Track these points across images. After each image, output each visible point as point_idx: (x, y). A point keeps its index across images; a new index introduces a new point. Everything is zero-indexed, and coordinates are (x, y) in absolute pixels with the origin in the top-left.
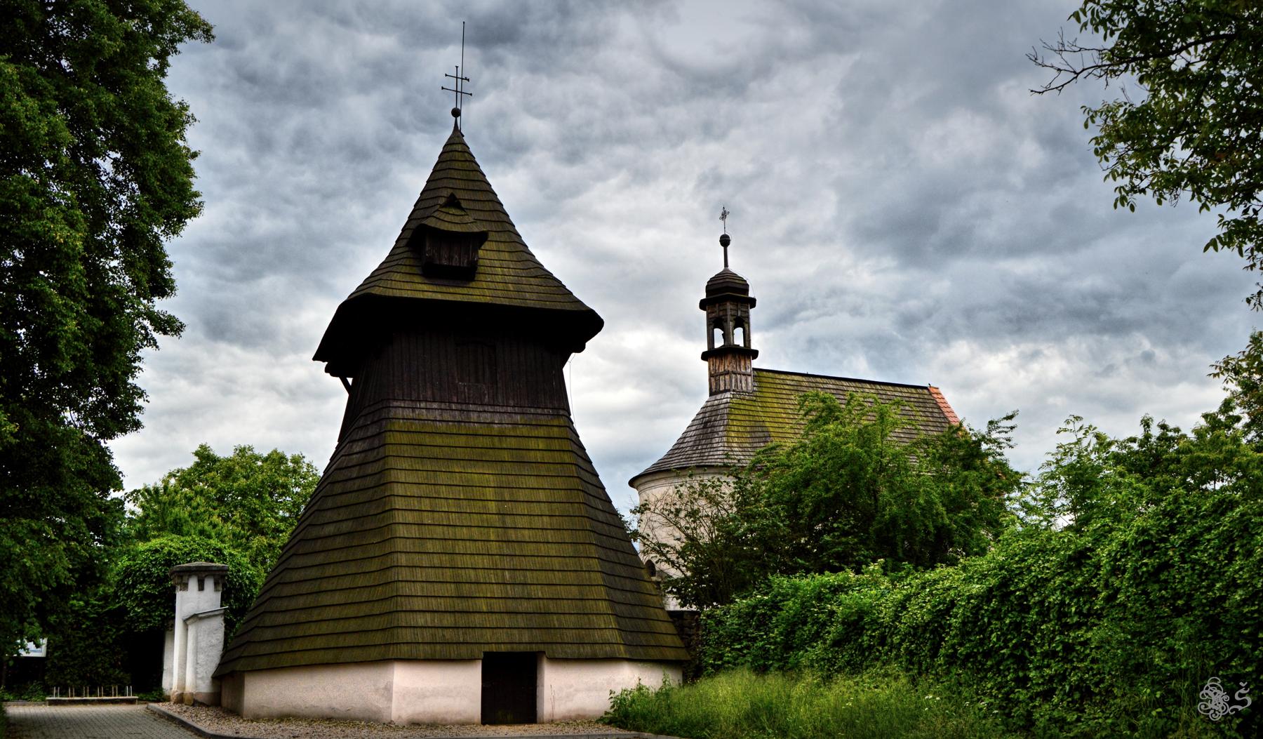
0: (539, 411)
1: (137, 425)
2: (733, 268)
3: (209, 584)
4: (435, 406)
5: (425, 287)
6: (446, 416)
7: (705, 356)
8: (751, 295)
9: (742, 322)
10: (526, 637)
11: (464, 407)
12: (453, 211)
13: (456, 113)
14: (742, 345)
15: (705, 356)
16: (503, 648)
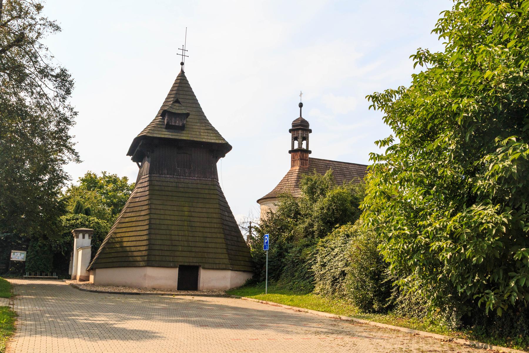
0: (206, 179)
1: (129, 154)
2: (304, 117)
3: (87, 236)
4: (168, 176)
5: (166, 133)
6: (172, 180)
7: (290, 152)
8: (310, 128)
9: (306, 138)
10: (195, 260)
11: (179, 177)
12: (177, 105)
13: (182, 64)
14: (305, 148)
15: (290, 152)
16: (186, 264)
